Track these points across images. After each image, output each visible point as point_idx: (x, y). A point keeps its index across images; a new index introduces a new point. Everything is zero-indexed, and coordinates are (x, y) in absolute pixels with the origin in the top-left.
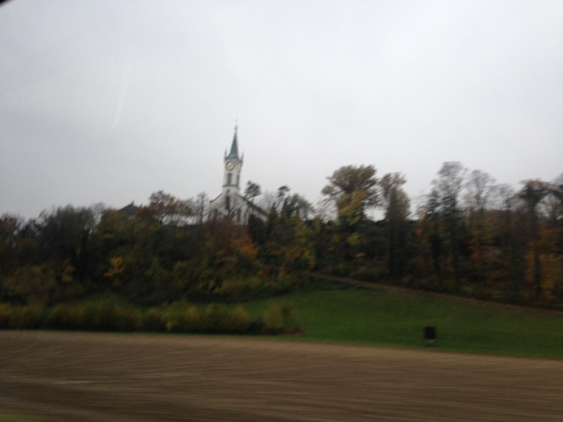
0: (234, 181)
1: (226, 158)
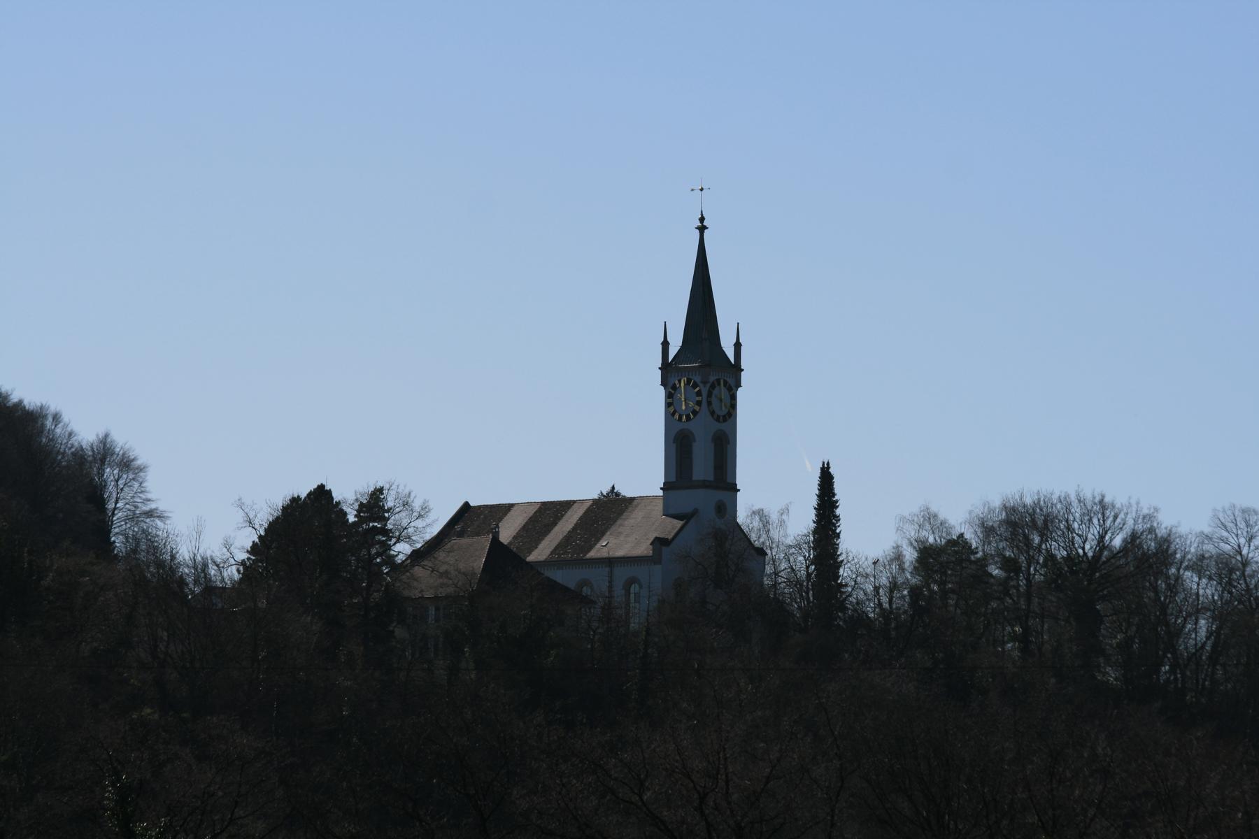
0: (702, 468)
1: (666, 367)
